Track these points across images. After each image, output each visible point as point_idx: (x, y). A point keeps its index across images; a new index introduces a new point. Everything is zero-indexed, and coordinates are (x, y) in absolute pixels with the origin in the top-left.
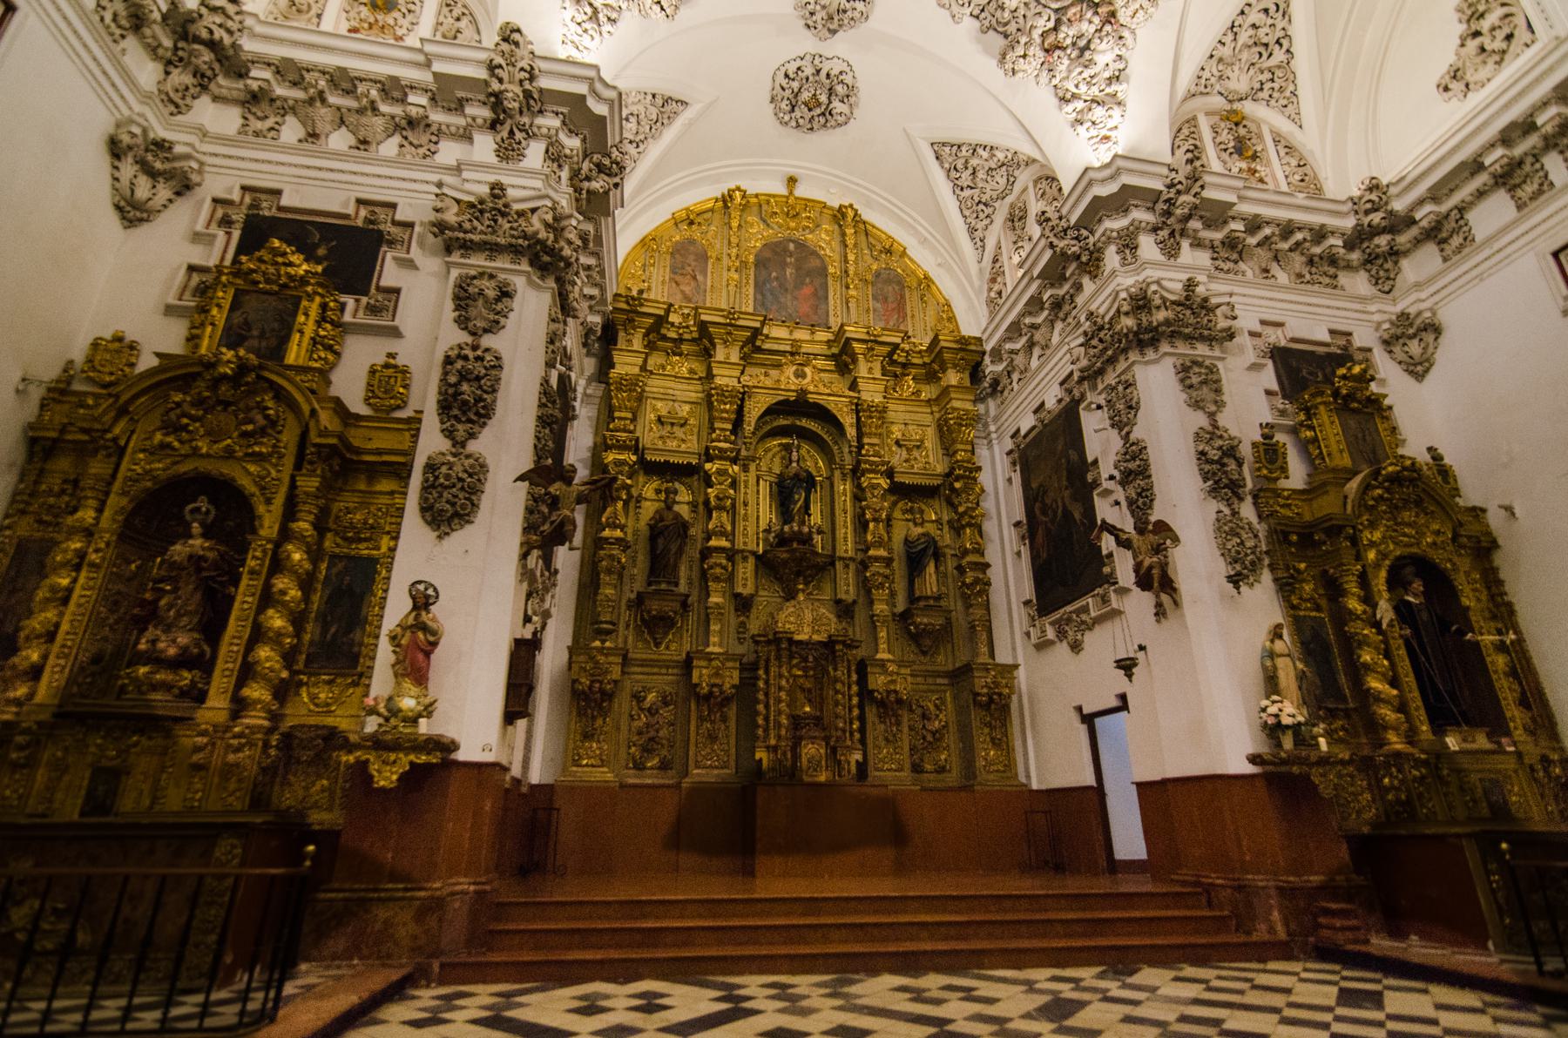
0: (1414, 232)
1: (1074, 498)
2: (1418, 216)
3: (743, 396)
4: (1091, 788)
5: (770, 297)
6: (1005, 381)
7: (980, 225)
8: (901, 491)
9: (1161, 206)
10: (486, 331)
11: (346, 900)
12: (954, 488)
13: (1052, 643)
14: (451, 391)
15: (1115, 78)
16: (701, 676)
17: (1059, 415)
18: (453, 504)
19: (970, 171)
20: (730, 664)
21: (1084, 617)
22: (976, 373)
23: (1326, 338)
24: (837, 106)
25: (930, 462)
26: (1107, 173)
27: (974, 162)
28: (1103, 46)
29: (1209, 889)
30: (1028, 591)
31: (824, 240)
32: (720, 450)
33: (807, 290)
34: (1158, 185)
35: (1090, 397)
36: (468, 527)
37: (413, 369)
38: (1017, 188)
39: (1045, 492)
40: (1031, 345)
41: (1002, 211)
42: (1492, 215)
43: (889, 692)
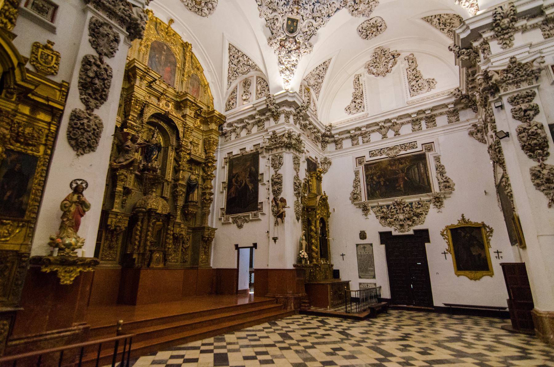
0: (332, 139)
1: (251, 182)
2: (335, 136)
3: (145, 105)
4: (235, 269)
5: (154, 65)
6: (228, 134)
7: (232, 78)
8: (191, 162)
9: (298, 110)
10: (106, 55)
11: (25, 343)
12: (206, 165)
13: (230, 223)
14: (89, 80)
15: (294, 66)
16: (112, 222)
17: (251, 154)
18: (88, 140)
19: (238, 60)
20: (125, 218)
21: (247, 219)
22: (220, 126)
23: (314, 158)
24: (205, 10)
25: (199, 153)
26: (291, 95)
27: (241, 59)
28: (295, 55)
29: (277, 299)
30: (224, 205)
31: (177, 50)
32: (132, 125)
33: (168, 69)
34: (300, 104)
35: (265, 154)
36: (92, 153)
37: (62, 55)
38: (249, 74)
39: (238, 176)
40: (244, 127)
41: (241, 78)
42: (347, 143)
43: (180, 234)
